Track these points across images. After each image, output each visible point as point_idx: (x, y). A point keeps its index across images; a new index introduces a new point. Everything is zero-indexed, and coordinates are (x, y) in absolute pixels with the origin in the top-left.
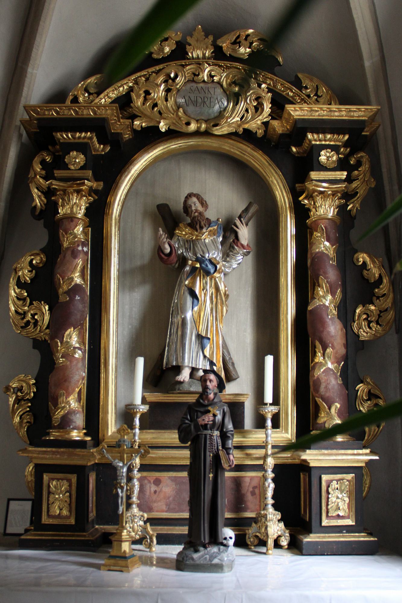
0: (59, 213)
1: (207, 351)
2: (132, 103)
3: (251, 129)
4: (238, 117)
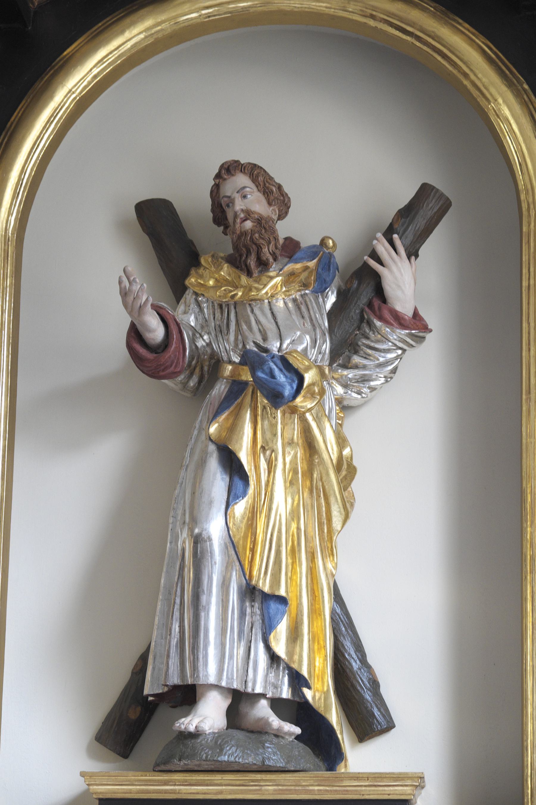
1: (277, 640)
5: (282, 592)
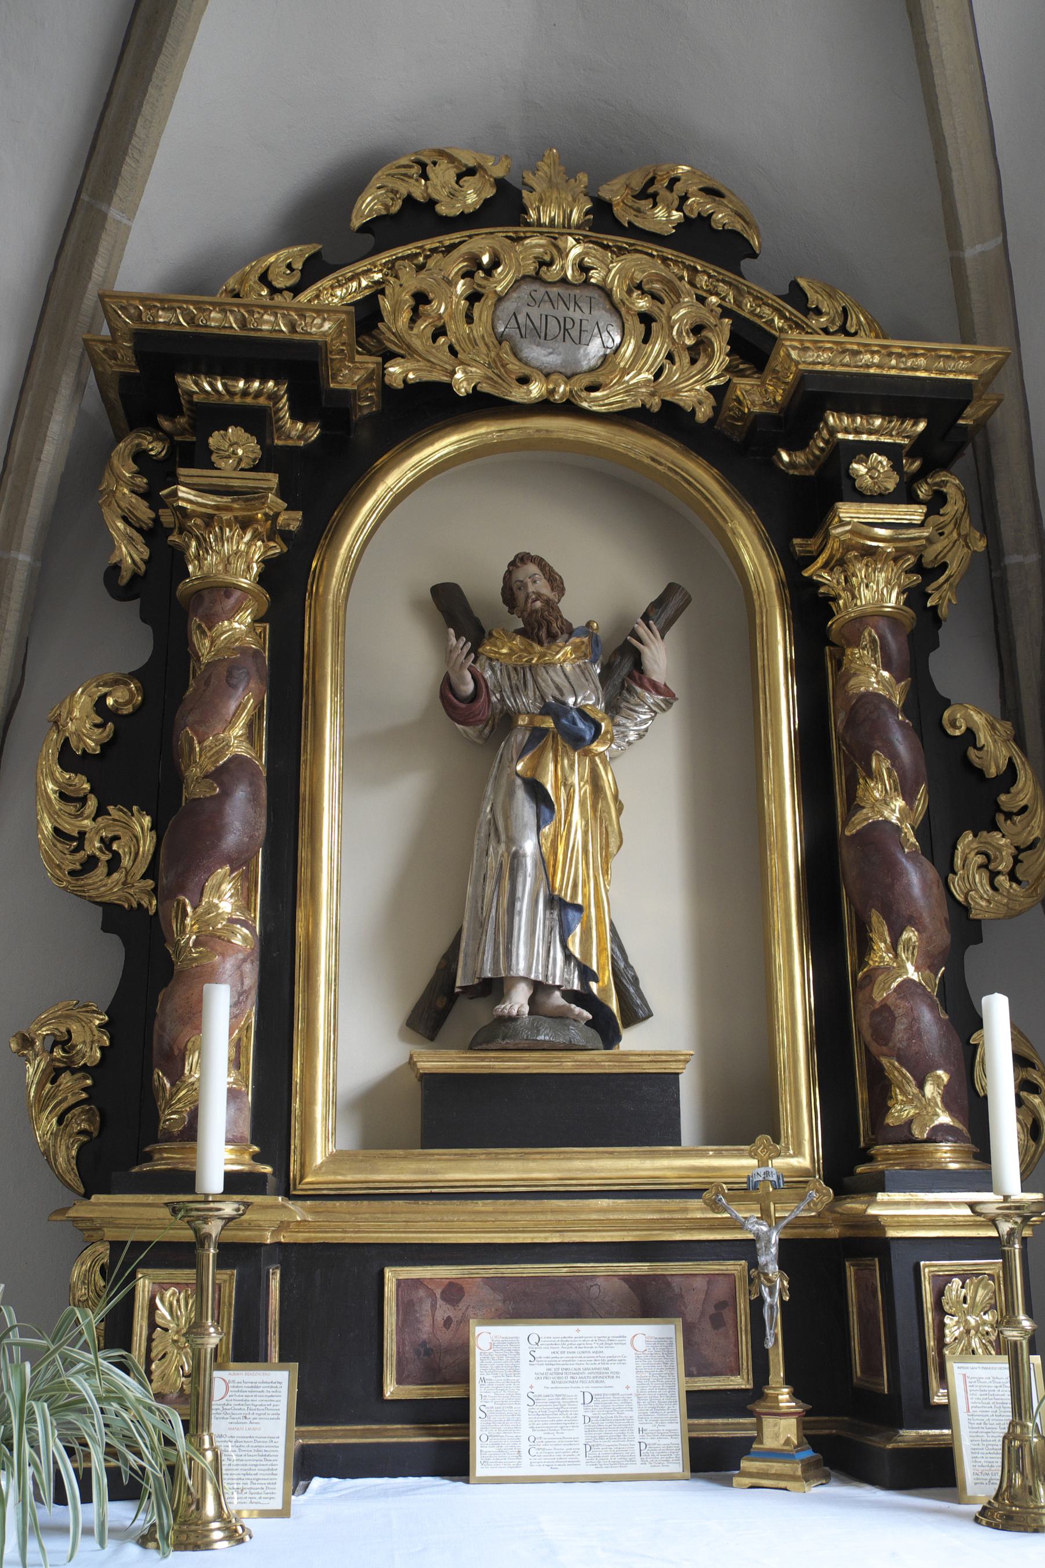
0: (187, 574)
1: (573, 942)
2: (383, 321)
3: (682, 404)
4: (648, 371)
5: (579, 901)
